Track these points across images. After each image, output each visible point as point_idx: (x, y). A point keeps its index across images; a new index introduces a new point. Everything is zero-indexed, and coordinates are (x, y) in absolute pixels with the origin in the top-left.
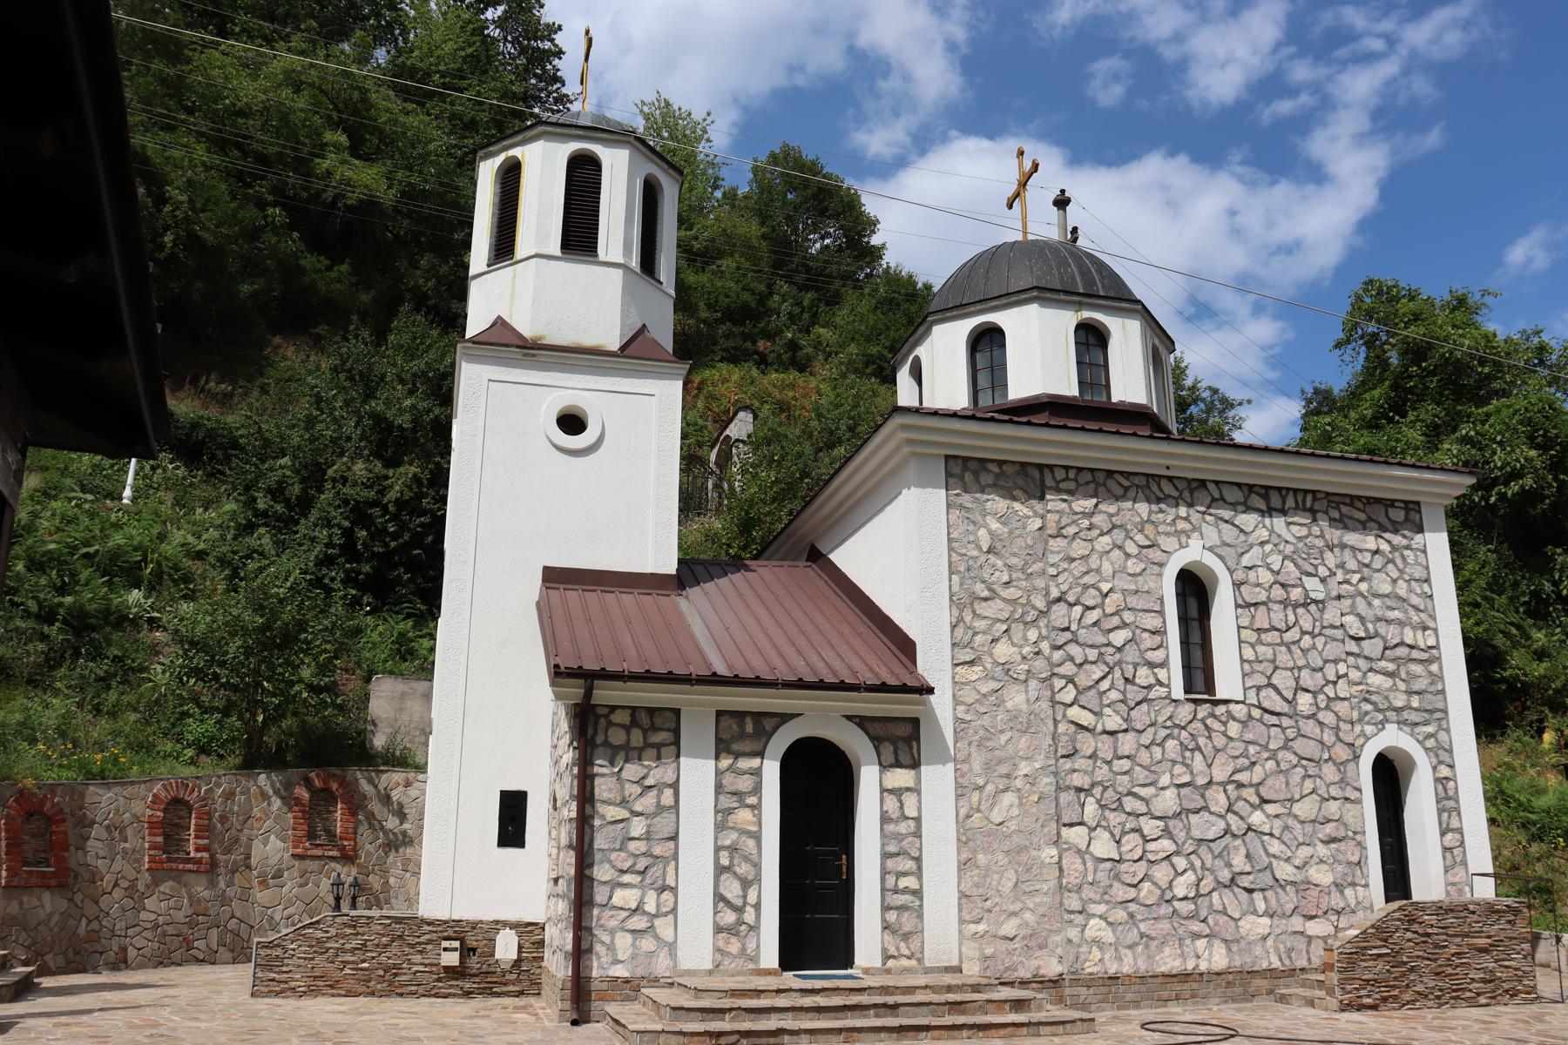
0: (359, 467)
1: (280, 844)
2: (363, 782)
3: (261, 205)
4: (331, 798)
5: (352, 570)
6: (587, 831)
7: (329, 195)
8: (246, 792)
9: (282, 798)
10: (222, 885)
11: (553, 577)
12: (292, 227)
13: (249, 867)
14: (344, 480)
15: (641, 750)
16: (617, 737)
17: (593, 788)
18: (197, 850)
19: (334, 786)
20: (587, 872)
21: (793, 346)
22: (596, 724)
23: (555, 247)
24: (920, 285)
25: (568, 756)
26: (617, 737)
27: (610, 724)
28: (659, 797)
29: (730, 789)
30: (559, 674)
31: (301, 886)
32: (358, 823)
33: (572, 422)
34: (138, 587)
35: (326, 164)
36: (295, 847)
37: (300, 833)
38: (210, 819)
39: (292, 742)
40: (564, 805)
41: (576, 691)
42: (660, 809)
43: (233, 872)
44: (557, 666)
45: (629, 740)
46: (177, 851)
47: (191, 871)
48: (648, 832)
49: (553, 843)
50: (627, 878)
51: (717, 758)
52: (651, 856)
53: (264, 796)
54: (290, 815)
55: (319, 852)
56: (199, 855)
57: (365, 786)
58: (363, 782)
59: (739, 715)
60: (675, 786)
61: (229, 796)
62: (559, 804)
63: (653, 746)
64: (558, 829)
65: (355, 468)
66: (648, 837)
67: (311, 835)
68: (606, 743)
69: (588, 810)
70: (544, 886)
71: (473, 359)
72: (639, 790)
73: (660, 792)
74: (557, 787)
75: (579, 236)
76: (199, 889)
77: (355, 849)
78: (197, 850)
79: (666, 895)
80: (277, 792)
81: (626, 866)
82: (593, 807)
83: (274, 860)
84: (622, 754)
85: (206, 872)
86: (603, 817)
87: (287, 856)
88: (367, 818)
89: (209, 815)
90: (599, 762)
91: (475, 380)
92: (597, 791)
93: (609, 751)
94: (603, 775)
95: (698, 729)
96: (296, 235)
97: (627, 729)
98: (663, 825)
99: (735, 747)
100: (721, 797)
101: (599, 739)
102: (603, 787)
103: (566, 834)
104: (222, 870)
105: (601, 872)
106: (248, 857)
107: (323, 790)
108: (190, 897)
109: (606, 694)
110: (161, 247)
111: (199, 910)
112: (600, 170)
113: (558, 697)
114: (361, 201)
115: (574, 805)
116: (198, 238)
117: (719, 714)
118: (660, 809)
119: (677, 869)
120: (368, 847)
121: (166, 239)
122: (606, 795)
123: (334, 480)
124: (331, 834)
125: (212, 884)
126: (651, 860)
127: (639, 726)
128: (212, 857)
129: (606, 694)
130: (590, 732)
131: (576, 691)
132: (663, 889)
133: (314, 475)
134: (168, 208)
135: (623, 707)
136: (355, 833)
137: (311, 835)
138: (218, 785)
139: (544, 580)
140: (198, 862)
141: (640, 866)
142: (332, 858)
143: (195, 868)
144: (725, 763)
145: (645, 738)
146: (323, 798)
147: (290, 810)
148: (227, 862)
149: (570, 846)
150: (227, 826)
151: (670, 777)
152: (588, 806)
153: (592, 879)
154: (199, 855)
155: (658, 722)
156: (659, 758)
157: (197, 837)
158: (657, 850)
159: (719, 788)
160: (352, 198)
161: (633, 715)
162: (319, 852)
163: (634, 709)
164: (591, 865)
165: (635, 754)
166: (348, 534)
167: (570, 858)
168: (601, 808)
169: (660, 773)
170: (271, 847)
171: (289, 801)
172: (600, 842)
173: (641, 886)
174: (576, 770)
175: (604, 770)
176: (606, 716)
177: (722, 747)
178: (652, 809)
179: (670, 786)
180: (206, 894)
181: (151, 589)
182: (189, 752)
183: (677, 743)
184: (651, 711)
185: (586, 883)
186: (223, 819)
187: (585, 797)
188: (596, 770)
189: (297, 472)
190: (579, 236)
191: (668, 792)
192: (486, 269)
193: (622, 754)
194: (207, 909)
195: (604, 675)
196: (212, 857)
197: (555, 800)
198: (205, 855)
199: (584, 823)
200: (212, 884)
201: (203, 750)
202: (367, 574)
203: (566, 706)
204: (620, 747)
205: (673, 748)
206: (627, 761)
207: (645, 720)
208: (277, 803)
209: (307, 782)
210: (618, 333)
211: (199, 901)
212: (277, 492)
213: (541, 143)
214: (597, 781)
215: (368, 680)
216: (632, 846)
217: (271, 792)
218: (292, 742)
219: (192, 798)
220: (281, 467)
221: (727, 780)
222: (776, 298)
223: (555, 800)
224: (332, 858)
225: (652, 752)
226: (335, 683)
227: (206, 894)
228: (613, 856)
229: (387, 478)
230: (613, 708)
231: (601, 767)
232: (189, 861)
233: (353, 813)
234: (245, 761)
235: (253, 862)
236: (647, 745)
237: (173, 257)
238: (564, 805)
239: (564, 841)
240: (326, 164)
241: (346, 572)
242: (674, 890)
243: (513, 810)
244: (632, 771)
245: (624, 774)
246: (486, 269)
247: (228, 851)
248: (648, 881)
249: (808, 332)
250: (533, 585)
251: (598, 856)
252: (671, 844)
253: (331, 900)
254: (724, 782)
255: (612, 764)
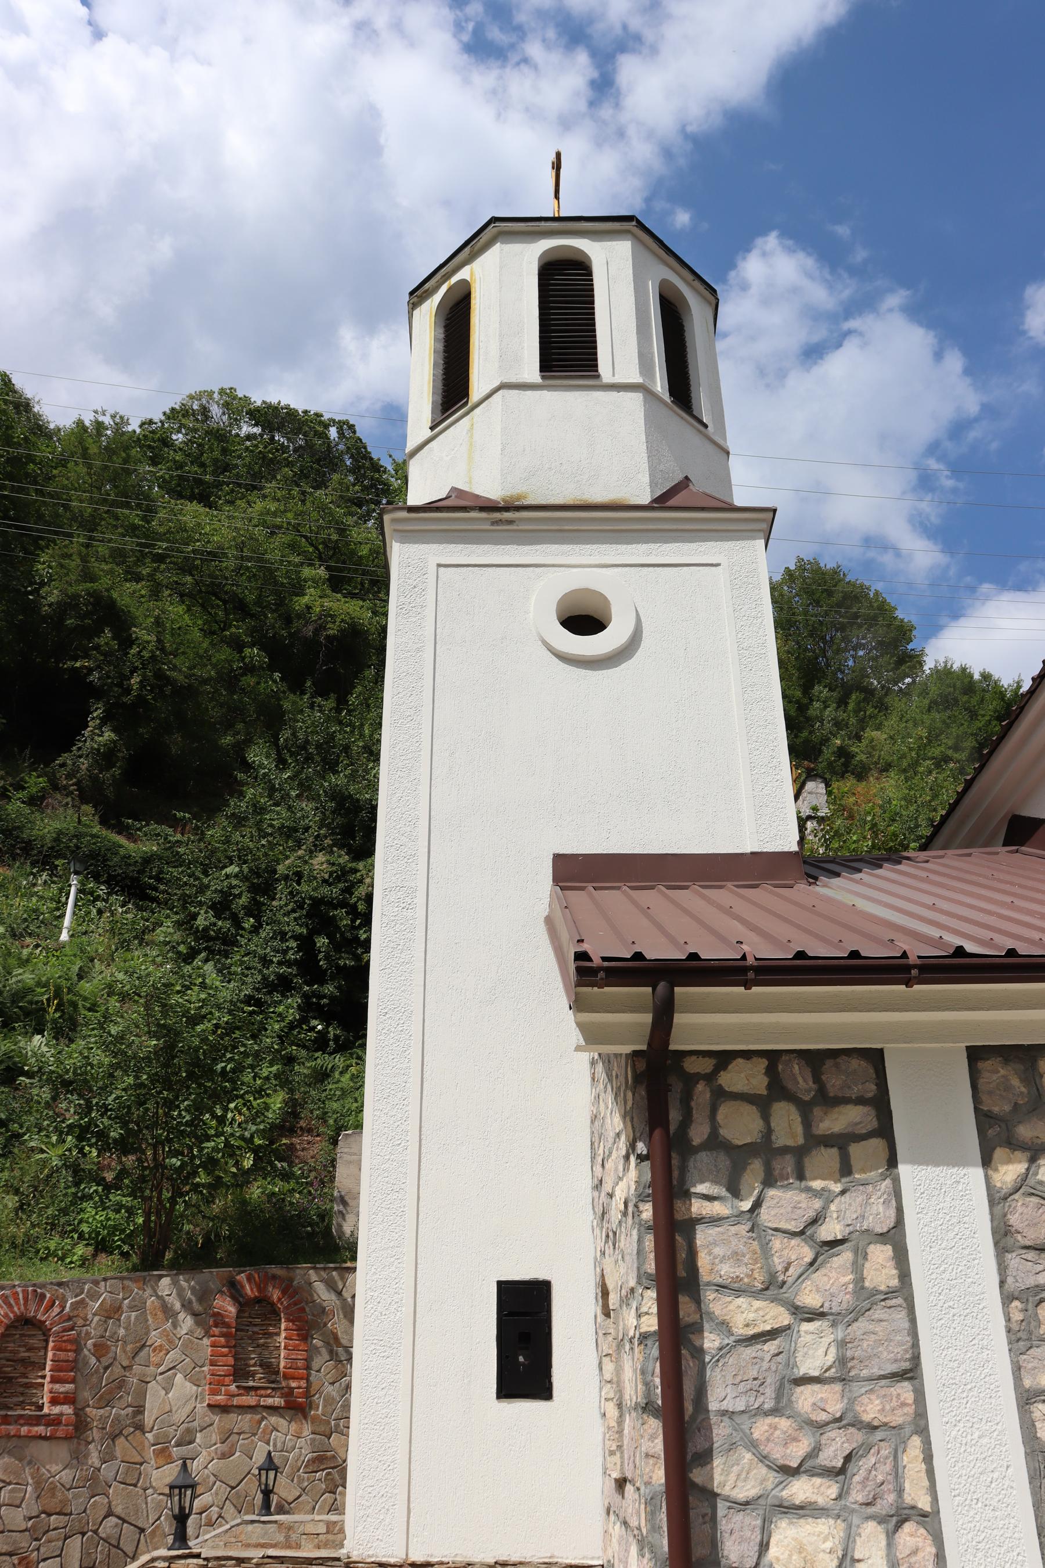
0: (320, 862)
1: (190, 1388)
2: (320, 1288)
3: (238, 646)
4: (271, 1314)
5: (314, 994)
6: (688, 1364)
7: (309, 631)
8: (139, 1306)
9: (195, 1314)
10: (94, 1459)
11: (573, 871)
12: (272, 668)
13: (140, 1427)
14: (299, 875)
15: (800, 1153)
16: (740, 1125)
17: (692, 1253)
18: (54, 1402)
19: (275, 1294)
20: (697, 1476)
21: (843, 753)
22: (687, 1097)
23: (530, 369)
24: (977, 676)
25: (628, 1180)
26: (740, 1125)
27: (720, 1095)
28: (857, 1268)
29: (1031, 1236)
30: (591, 975)
31: (224, 1456)
32: (311, 1353)
33: (583, 621)
34: (40, 1032)
35: (305, 600)
36: (213, 1392)
37: (222, 1370)
38: (78, 1351)
39: (225, 1231)
40: (625, 1301)
41: (631, 1017)
42: (866, 1299)
43: (114, 1438)
44: (581, 956)
45: (768, 1132)
46: (21, 1405)
47: (40, 1437)
48: (842, 1361)
49: (609, 1391)
50: (801, 1490)
51: (987, 1161)
52: (857, 1424)
53: (168, 1312)
54: (206, 1341)
55: (250, 1400)
56: (56, 1410)
57: (323, 1294)
58: (320, 1288)
59: (1024, 1056)
60: (895, 1236)
61: (112, 1312)
62: (613, 1300)
63: (828, 1141)
64: (615, 1355)
65: (314, 862)
66: (841, 1374)
67: (240, 1373)
68: (715, 1142)
69: (686, 1308)
70: (595, 1489)
71: (409, 536)
72: (808, 1254)
73: (861, 1255)
74: (608, 1263)
75: (567, 346)
76: (54, 1468)
77: (307, 1394)
78: (54, 1402)
79: (911, 1536)
80: (186, 1306)
81: (795, 1454)
82: (698, 1301)
83: (180, 1415)
84: (756, 1166)
85: (67, 1438)
86: (724, 1326)
87: (201, 1407)
88: (327, 1344)
89: (77, 1345)
90: (701, 1188)
91: (410, 563)
92: (703, 1261)
93: (724, 1161)
94: (715, 1221)
95: (931, 1097)
96: (277, 675)
97: (763, 1104)
98: (878, 1339)
99: (1025, 1131)
100: (1013, 1260)
101: (698, 1133)
102: (718, 1252)
103: (637, 1373)
104: (96, 1434)
105: (733, 1476)
106: (140, 1410)
107: (258, 1301)
108: (38, 1484)
109: (708, 1021)
110: (128, 691)
111: (52, 1506)
112: (590, 274)
113: (591, 1036)
114: (341, 631)
115: (650, 1301)
116: (167, 678)
117: (976, 1055)
118: (866, 1299)
119: (928, 1458)
120: (329, 1389)
121: (133, 681)
122: (726, 1271)
123: (286, 878)
124: (270, 1370)
125: (78, 1458)
126: (857, 1437)
127: (789, 1096)
128: (79, 1413)
129: (708, 1021)
130: (675, 1116)
131: (631, 1017)
132: (901, 1516)
133: (262, 884)
134: (134, 650)
135: (747, 1055)
136: (308, 1368)
137: (240, 1373)
138: (94, 1296)
139: (557, 879)
140: (54, 1421)
141: (832, 1454)
142: (273, 1409)
143: (47, 1431)
144: (1009, 1171)
145: (807, 1124)
146: (258, 1313)
147: (208, 1334)
148: (103, 1419)
149: (647, 1407)
150: (105, 1361)
151: (880, 1217)
152: (683, 1299)
153: (711, 1496)
154: (56, 1410)
155: (834, 1082)
156: (846, 1170)
157: (54, 1380)
158: (871, 1409)
159: (1003, 1237)
160: (332, 630)
161: (771, 1071)
162: (250, 1400)
163: (773, 1057)
164: (705, 1457)
165: (787, 1163)
166: (306, 944)
167: (651, 1437)
168: (716, 1304)
169: (855, 1208)
170: (176, 1392)
171: (207, 1319)
172: (722, 1393)
173: (838, 1510)
174: (647, 1212)
175: (717, 1208)
176: (710, 1077)
177: (995, 1135)
178: (845, 1300)
179: (883, 1237)
180: (66, 1476)
181: (58, 1034)
182: (80, 1250)
183: (885, 1130)
184: (815, 1060)
185: (697, 1508)
186: (100, 1350)
187: (676, 1279)
188: (698, 1207)
189: (246, 879)
190: (567, 346)
191: (880, 1255)
192: (429, 433)
193: (756, 1166)
194: (65, 1502)
195: (696, 971)
196: (79, 1413)
197: (605, 1293)
198: (67, 1409)
199: (677, 1342)
200: (78, 1458)
201: (101, 1246)
202: (332, 998)
203: (607, 1060)
204: (750, 1150)
205: (877, 1144)
206: (769, 1182)
207: (802, 1082)
208: (187, 1322)
209: (233, 1288)
210: (646, 479)
211: (53, 1489)
212: (222, 907)
213: (497, 248)
214: (703, 1236)
215: (335, 1142)
216: (806, 1398)
217: (178, 1306)
218: (225, 1231)
219: (48, 1317)
220: (228, 876)
221: (1022, 1213)
222: (817, 705)
223: (605, 1293)
224: (273, 1409)
225: (829, 1156)
226: (291, 1147)
227: (66, 1476)
228: (760, 1429)
229: (356, 871)
230: (724, 1059)
231: (707, 1199)
232: (37, 1420)
233: (305, 1337)
234: (143, 1260)
235: (148, 1418)
236: (815, 1141)
237: (141, 700)
238: (625, 1301)
239: (633, 1393)
240: (305, 600)
241: (306, 996)
242: (929, 1519)
243: (524, 1320)
244: (784, 1206)
245: (767, 1216)
246: (429, 433)
247: (106, 1402)
248: (857, 1496)
249: (859, 738)
250: (540, 885)
251: (721, 1432)
252: (905, 1391)
253: (167, 1526)
254: (1014, 1219)
255: (735, 1191)
